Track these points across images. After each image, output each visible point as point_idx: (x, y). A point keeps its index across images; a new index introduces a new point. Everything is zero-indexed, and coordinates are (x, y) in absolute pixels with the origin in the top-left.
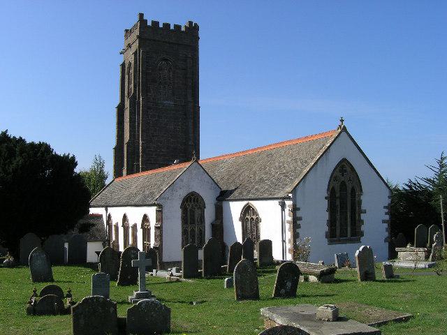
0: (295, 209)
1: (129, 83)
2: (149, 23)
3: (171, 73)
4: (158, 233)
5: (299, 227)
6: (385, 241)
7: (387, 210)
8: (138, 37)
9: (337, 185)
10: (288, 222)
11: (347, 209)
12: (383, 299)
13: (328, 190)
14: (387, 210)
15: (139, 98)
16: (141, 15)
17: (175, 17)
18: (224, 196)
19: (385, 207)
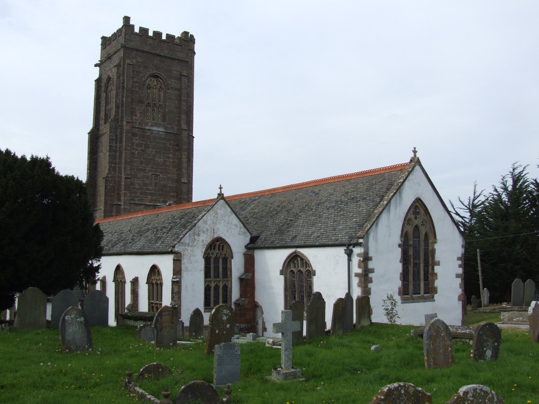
0: (366, 258)
1: (107, 104)
2: (137, 30)
3: (162, 94)
6: (459, 300)
7: (460, 262)
9: (410, 229)
10: (357, 275)
14: (460, 262)
16: (127, 19)
17: (166, 23)
19: (459, 259)
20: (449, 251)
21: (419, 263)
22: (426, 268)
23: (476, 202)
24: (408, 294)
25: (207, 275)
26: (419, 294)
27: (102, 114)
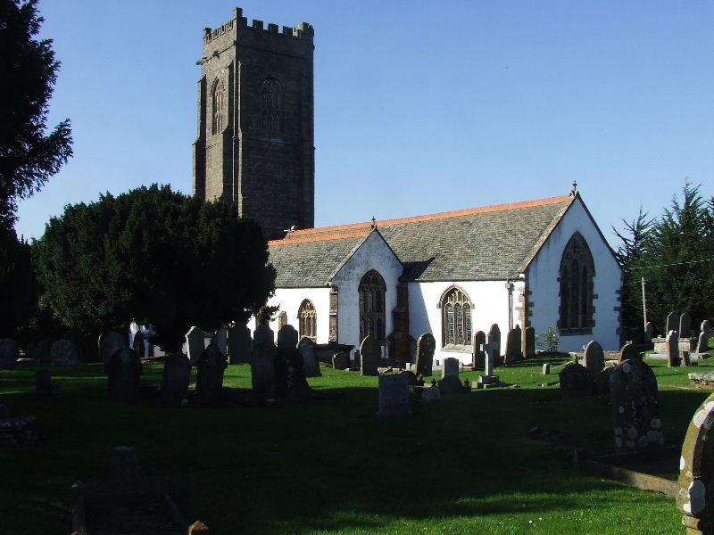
0: (527, 293)
1: (215, 110)
4: (334, 324)
8: (236, 43)
10: (517, 309)
12: (633, 407)
15: (237, 133)
16: (239, 11)
18: (412, 272)
19: (617, 292)
20: (606, 284)
23: (641, 222)
27: (209, 122)
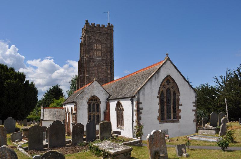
0: (139, 103)
5: (141, 113)
9: (165, 90)
10: (135, 111)
11: (170, 103)
13: (159, 92)
16: (87, 21)
17: (103, 22)
19: (193, 103)
21: (171, 105)
22: (175, 107)
24: (164, 119)
25: (89, 110)
26: (171, 119)
